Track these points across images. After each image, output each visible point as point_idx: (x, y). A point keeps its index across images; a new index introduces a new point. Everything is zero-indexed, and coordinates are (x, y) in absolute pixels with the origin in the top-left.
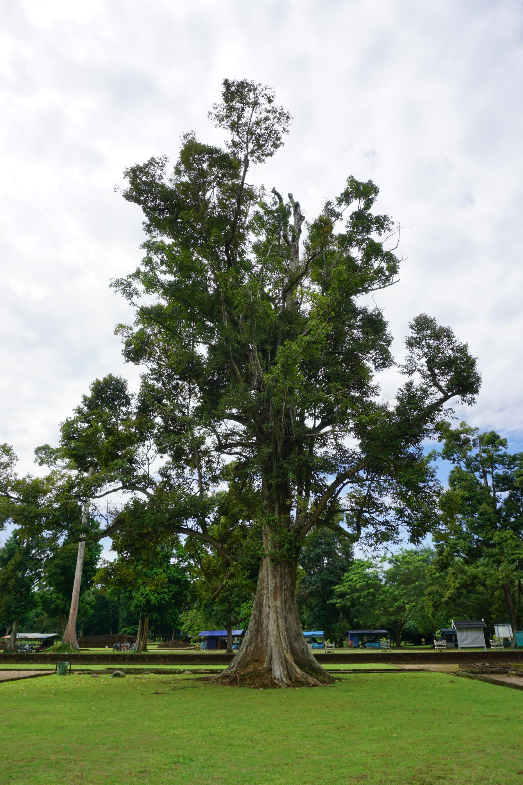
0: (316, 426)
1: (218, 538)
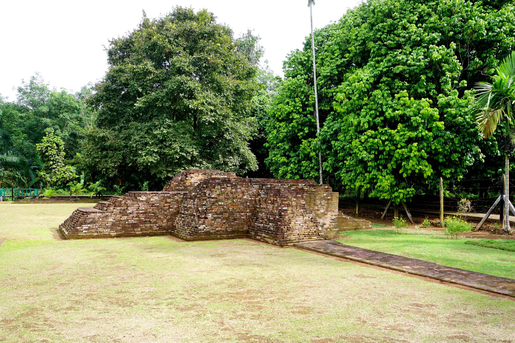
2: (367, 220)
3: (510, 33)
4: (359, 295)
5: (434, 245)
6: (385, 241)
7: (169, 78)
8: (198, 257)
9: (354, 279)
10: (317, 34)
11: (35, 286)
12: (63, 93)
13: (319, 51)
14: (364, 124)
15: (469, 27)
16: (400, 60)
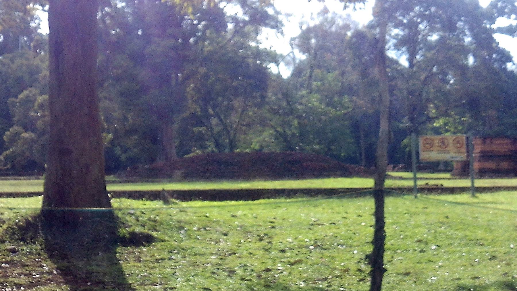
0: (115, 203)
1: (477, 171)
2: (286, 199)
3: (510, 31)
4: (224, 120)
5: (501, 196)
6: (330, 193)
7: (126, 260)
8: (275, 208)
9: (166, 238)
10: (445, 141)
11: (440, 67)
12: (300, 52)
13: (127, 78)
14: (446, 120)
15: (52, 105)
16: (127, 221)
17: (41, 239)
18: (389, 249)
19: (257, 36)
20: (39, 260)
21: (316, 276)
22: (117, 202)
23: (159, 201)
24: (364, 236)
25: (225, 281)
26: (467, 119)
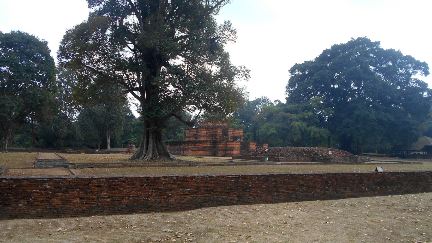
12: (395, 50)
17: (306, 144)
18: (38, 154)
19: (225, 57)
20: (117, 72)
21: (134, 77)
22: (414, 199)
23: (288, 85)
24: (217, 209)
25: (242, 118)
26: (376, 118)
